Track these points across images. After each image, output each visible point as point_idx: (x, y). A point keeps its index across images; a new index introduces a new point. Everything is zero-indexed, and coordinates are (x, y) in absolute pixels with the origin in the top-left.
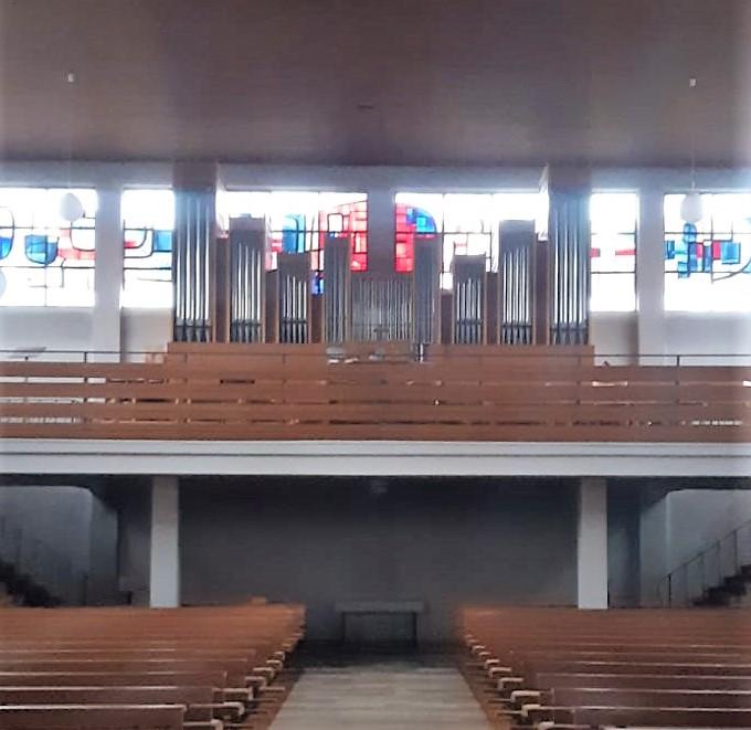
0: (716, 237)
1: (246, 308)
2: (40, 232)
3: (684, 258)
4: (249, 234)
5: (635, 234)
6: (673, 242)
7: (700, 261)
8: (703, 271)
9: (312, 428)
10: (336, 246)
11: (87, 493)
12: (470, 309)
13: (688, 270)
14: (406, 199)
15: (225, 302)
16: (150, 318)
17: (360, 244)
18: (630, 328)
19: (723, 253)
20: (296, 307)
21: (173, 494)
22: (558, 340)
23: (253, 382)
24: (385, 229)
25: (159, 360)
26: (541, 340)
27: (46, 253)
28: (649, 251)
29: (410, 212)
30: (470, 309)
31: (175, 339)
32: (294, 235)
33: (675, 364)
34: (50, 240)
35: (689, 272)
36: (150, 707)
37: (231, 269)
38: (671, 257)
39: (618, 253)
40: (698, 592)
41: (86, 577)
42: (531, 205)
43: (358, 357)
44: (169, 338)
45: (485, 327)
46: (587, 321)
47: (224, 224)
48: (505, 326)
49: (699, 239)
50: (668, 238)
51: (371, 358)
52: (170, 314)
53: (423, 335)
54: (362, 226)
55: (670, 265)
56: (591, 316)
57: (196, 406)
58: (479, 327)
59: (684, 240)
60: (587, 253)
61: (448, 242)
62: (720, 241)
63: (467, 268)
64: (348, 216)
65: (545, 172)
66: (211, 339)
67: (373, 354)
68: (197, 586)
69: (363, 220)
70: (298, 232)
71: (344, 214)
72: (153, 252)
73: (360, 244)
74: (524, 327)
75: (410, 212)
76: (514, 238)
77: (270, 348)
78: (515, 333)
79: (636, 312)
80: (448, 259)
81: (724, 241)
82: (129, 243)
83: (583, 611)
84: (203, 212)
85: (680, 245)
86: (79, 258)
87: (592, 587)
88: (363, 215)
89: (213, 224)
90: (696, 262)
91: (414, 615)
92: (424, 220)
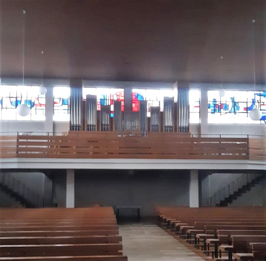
0: (222, 103)
1: (92, 121)
2: (29, 99)
3: (213, 109)
4: (92, 100)
5: (199, 102)
6: (210, 104)
7: (217, 109)
8: (218, 112)
9: (111, 155)
10: (117, 103)
11: (43, 175)
12: (155, 122)
13: (214, 112)
14: (135, 91)
15: (85, 119)
16: (62, 124)
17: (123, 103)
18: (198, 127)
19: (224, 107)
20: (106, 121)
21: (73, 175)
22: (180, 131)
23: (97, 142)
24: (129, 100)
25: (66, 135)
26: (176, 131)
27: (31, 104)
28: (203, 106)
29: (136, 95)
30: (155, 122)
31: (71, 129)
32: (103, 101)
33: (219, 137)
34: (32, 101)
35: (214, 113)
36: (80, 245)
37: (87, 110)
38: (209, 108)
39: (195, 107)
40: (219, 202)
41: (44, 199)
42: (173, 93)
43: (127, 134)
44: (69, 129)
45: (82, 128)
46: (189, 126)
47: (84, 97)
48: (166, 127)
49: (217, 103)
50: (209, 103)
51: (130, 135)
52: (69, 122)
53: (143, 129)
54: (123, 98)
55: (209, 110)
56: (190, 124)
57: (61, 148)
58: (108, 126)
59: (213, 104)
60: (188, 108)
61: (148, 102)
62: (223, 104)
63: (155, 110)
64: (119, 95)
65: (176, 83)
66: (81, 130)
67: (131, 134)
68: (79, 203)
69: (123, 96)
70: (104, 100)
71: (117, 95)
72: (62, 104)
73: (123, 103)
74: (171, 127)
75: (136, 95)
76: (168, 102)
77: (99, 132)
78: (168, 128)
79: (200, 123)
80: (148, 107)
81: (224, 104)
82: (55, 102)
83: (191, 208)
84: (79, 94)
85: (212, 105)
86: (41, 106)
87: (194, 202)
88: (123, 95)
89: (82, 98)
90: (216, 110)
91: (139, 209)
92: (140, 97)
